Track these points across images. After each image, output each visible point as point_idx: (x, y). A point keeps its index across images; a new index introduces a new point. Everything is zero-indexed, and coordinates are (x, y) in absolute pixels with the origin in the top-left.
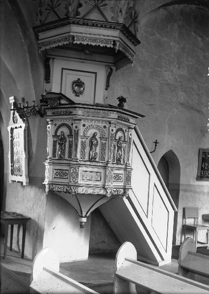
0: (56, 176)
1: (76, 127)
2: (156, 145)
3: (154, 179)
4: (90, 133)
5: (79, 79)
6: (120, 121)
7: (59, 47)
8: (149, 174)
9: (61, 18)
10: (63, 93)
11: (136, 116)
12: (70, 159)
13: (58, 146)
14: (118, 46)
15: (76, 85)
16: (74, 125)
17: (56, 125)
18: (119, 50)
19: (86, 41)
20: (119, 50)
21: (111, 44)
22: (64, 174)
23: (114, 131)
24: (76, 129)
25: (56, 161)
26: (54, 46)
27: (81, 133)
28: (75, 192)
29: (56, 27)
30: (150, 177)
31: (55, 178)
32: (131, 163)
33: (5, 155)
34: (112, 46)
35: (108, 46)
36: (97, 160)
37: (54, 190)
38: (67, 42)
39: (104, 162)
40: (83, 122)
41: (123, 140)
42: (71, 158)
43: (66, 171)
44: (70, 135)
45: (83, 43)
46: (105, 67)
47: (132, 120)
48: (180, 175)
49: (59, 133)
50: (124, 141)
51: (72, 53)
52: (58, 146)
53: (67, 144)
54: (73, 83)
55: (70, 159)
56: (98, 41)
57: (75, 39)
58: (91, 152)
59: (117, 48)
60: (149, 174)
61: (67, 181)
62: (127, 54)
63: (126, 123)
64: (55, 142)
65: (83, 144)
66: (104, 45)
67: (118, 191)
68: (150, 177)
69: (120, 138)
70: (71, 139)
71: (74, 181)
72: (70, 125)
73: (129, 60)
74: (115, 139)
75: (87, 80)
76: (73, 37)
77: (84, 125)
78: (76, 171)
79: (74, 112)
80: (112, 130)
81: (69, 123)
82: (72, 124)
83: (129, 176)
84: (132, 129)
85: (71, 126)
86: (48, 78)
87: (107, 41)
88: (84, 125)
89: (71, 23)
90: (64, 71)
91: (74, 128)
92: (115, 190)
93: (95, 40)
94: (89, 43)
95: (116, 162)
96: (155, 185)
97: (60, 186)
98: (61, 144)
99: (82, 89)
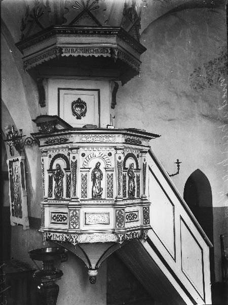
0: (53, 221)
1: (74, 158)
2: (178, 166)
3: (180, 211)
4: (92, 165)
5: (79, 99)
6: (130, 146)
7: (45, 63)
8: (173, 205)
9: (45, 27)
10: (61, 117)
11: (150, 137)
12: (68, 198)
13: (54, 182)
14: (116, 54)
15: (77, 106)
16: (71, 156)
18: (118, 59)
19: (77, 52)
20: (118, 59)
21: (107, 52)
22: (62, 218)
23: (123, 158)
24: (74, 161)
25: (52, 202)
26: (40, 62)
27: (80, 165)
28: (76, 242)
29: (40, 41)
30: (174, 209)
31: (52, 223)
32: (147, 195)
33: (5, 192)
34: (109, 56)
35: (105, 55)
36: (103, 196)
37: (52, 239)
38: (54, 56)
39: (111, 199)
40: (81, 151)
41: (135, 167)
42: (70, 197)
43: (65, 215)
44: (67, 169)
45: (73, 54)
46: (110, 82)
47: (144, 143)
48: (206, 177)
49: (54, 167)
50: (138, 169)
52: (54, 182)
53: (64, 179)
54: (73, 104)
55: (68, 198)
56: (92, 51)
57: (63, 51)
58: (94, 187)
59: (116, 57)
60: (173, 205)
61: (66, 227)
62: (130, 63)
63: (137, 147)
64: (50, 179)
65: (84, 178)
66: (100, 55)
67: (133, 235)
68: (174, 209)
69: (131, 165)
70: (69, 173)
71: (74, 228)
72: (66, 155)
73: (135, 69)
74: (125, 168)
75: (88, 98)
76: (61, 49)
77: (83, 155)
78: (76, 214)
79: (71, 140)
80: (120, 158)
81: (65, 153)
82: (69, 154)
83: (146, 212)
84: (146, 152)
85: (68, 157)
86: (43, 102)
88: (83, 155)
89: (56, 33)
90: (61, 91)
91: (71, 159)
92: (129, 233)
93: (86, 50)
94: (81, 54)
95: (127, 197)
96: (181, 218)
97: (58, 234)
98: (57, 180)
99: (83, 110)
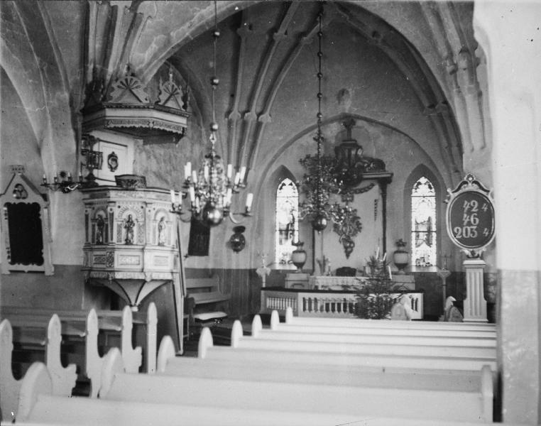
1: (111, 210)
5: (113, 153)
16: (109, 208)
17: (93, 208)
27: (116, 216)
40: (153, 206)
51: (251, 160)
87: (178, 128)
93: (169, 127)
